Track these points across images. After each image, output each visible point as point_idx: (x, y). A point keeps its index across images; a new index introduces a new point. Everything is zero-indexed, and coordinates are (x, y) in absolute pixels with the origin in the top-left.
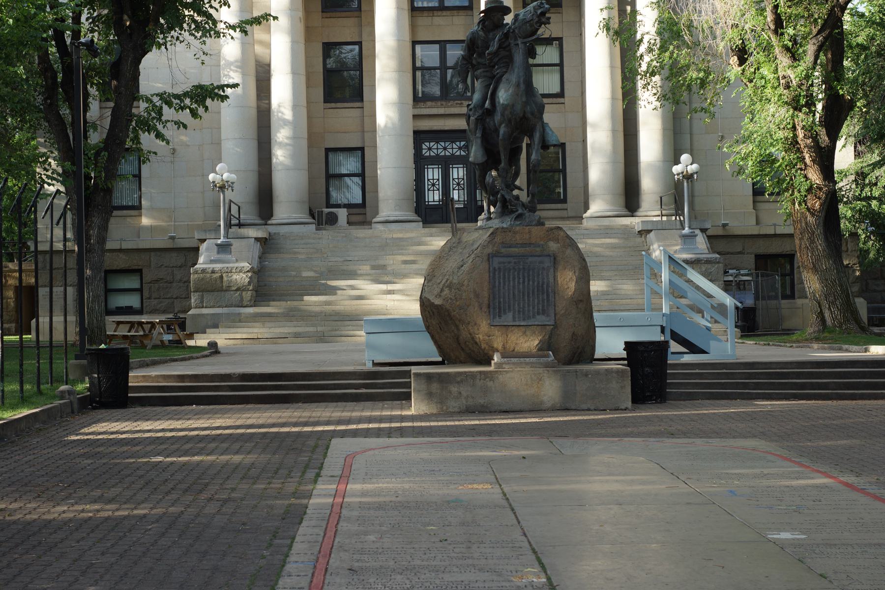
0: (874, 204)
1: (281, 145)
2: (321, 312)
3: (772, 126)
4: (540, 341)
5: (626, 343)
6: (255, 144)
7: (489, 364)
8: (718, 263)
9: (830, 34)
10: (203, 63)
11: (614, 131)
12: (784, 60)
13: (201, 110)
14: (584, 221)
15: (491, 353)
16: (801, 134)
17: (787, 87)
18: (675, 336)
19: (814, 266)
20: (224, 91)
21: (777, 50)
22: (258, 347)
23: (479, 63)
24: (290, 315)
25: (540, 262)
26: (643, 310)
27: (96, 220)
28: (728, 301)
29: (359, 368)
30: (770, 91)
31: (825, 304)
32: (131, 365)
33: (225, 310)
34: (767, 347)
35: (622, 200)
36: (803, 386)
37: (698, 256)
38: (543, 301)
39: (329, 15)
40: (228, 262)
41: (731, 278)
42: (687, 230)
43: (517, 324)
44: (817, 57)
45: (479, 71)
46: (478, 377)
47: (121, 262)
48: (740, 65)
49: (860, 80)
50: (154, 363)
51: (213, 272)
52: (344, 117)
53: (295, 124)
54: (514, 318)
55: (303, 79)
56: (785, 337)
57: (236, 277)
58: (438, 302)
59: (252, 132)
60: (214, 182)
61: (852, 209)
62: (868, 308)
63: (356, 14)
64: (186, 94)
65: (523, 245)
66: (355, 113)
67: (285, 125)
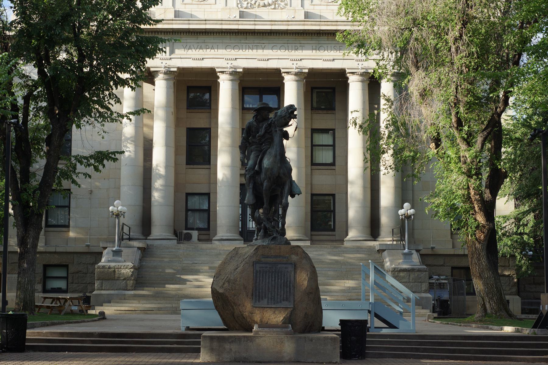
0: (525, 237)
1: (157, 190)
2: (176, 295)
3: (454, 187)
4: (284, 318)
5: (341, 320)
6: (141, 189)
7: (251, 331)
8: (426, 271)
9: (491, 131)
10: (103, 138)
11: (364, 187)
12: (463, 146)
13: (101, 167)
14: (345, 243)
15: (253, 324)
16: (472, 192)
17: (465, 163)
18: (377, 316)
19: (480, 275)
20: (115, 156)
21: (458, 140)
22: (134, 316)
23: (253, 142)
24: (156, 296)
25: (286, 268)
26: (360, 299)
27: (32, 233)
28: (411, 295)
29: (179, 332)
30: (454, 165)
31: (487, 299)
32: (28, 326)
33: (116, 292)
34: (446, 325)
35: (369, 230)
36: (454, 351)
37: (413, 267)
38: (287, 292)
39: (191, 111)
40: (119, 262)
41: (434, 281)
42: (406, 250)
43: (270, 306)
44: (483, 144)
45: (253, 147)
46: (243, 340)
47: (55, 260)
48: (436, 148)
49: (517, 160)
50: (53, 324)
51: (109, 268)
52: (198, 174)
53: (166, 177)
54: (268, 302)
55: (173, 150)
56: (461, 319)
57: (123, 271)
58: (221, 291)
59: (140, 182)
60: (112, 212)
61: (511, 240)
62: (522, 303)
64: (91, 157)
65: (276, 257)
66: (206, 171)
67: (160, 178)
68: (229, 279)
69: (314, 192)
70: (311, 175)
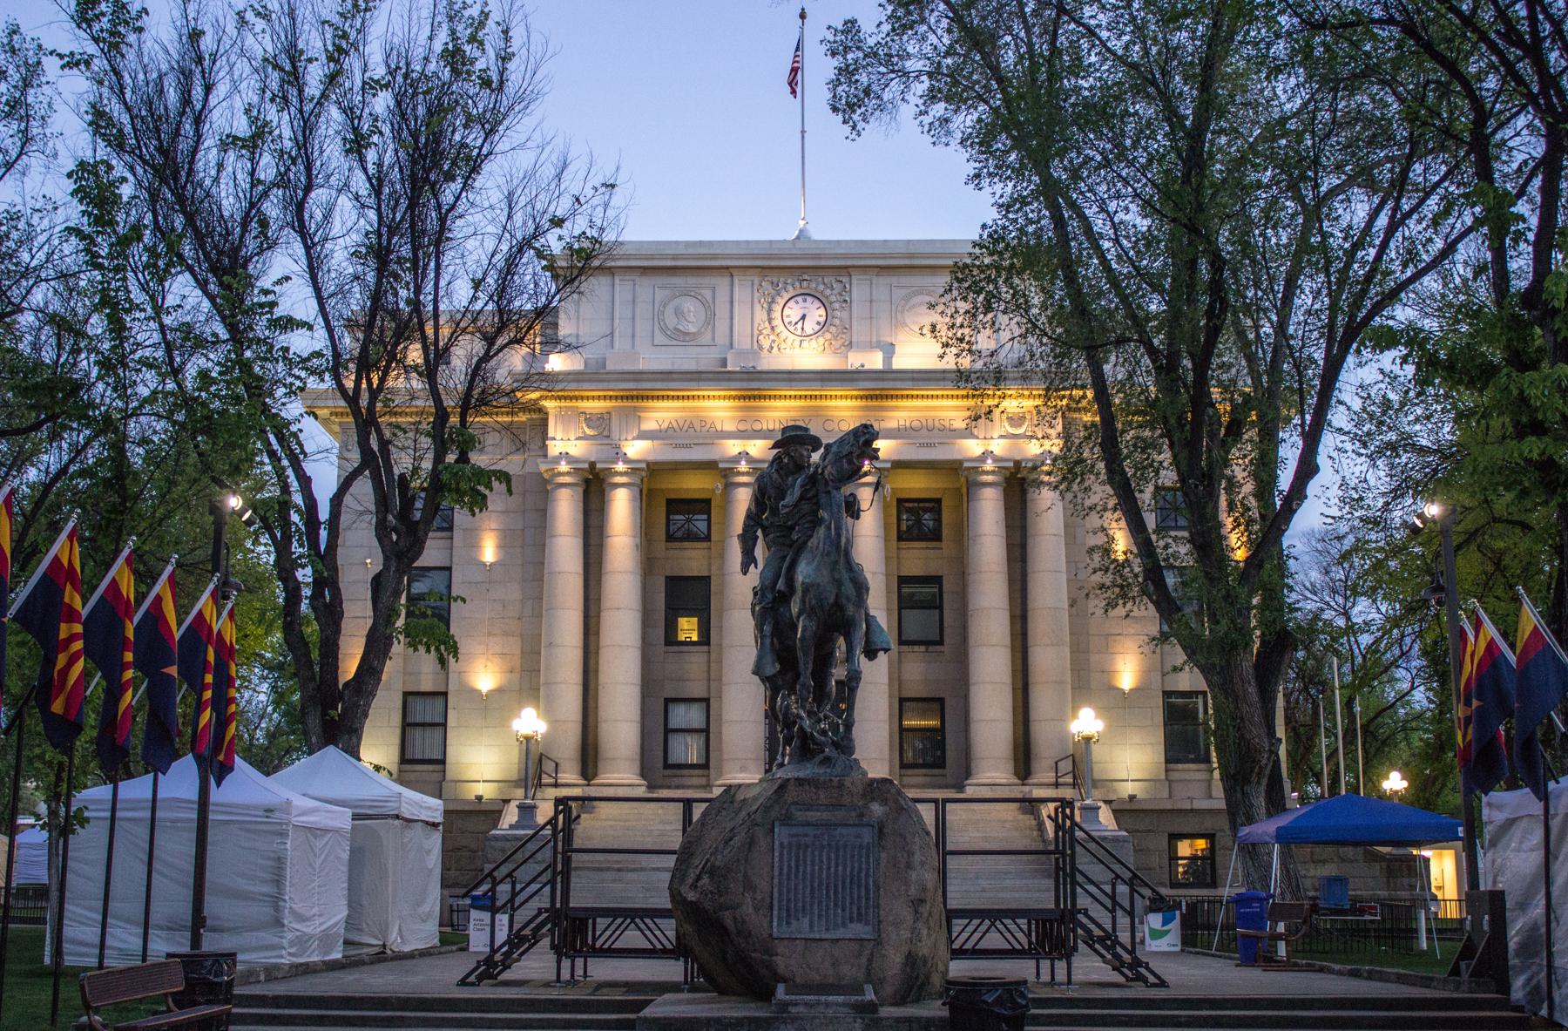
54: (811, 926)
58: (691, 896)
63: (705, 545)
68: (713, 866)
69: (906, 694)
70: (900, 661)
